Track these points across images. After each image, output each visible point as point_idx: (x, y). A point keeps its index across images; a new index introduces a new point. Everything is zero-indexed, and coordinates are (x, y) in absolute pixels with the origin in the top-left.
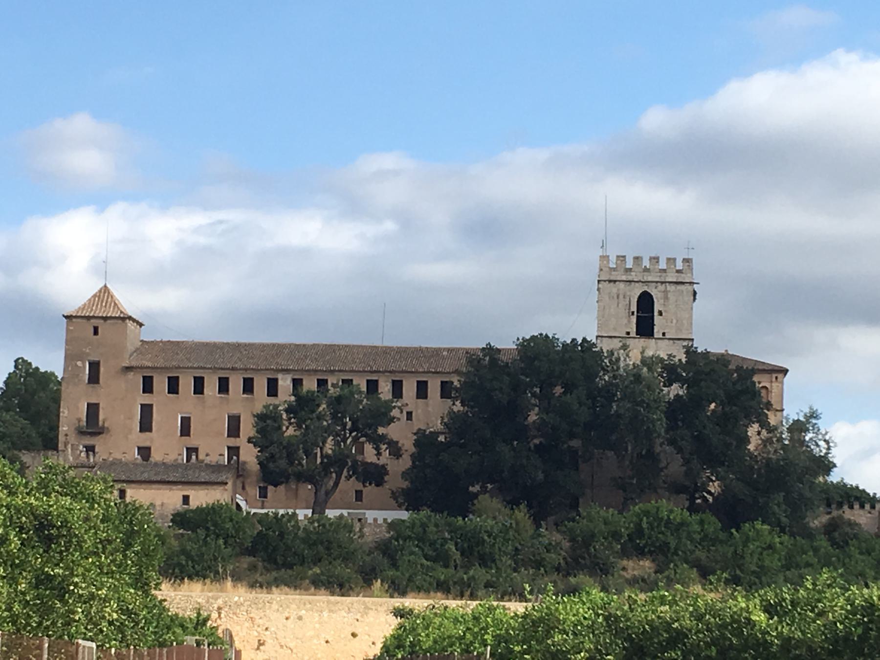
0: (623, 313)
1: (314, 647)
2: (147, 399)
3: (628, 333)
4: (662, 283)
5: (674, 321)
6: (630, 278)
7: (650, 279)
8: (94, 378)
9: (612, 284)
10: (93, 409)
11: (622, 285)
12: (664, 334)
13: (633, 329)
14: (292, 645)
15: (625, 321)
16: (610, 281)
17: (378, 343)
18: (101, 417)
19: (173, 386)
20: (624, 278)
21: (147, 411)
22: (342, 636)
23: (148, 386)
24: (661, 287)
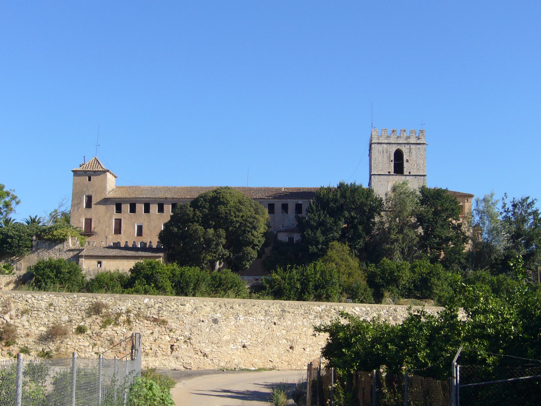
0: (386, 160)
1: (231, 352)
2: (118, 216)
3: (389, 172)
4: (408, 144)
5: (416, 165)
6: (389, 141)
7: (401, 142)
8: (89, 205)
9: (379, 145)
10: (89, 222)
11: (385, 146)
12: (410, 173)
13: (392, 170)
14: (207, 351)
15: (387, 166)
16: (378, 143)
17: (246, 186)
18: (93, 226)
19: (133, 209)
20: (386, 141)
21: (119, 222)
22: (260, 340)
23: (119, 209)
24: (407, 146)
